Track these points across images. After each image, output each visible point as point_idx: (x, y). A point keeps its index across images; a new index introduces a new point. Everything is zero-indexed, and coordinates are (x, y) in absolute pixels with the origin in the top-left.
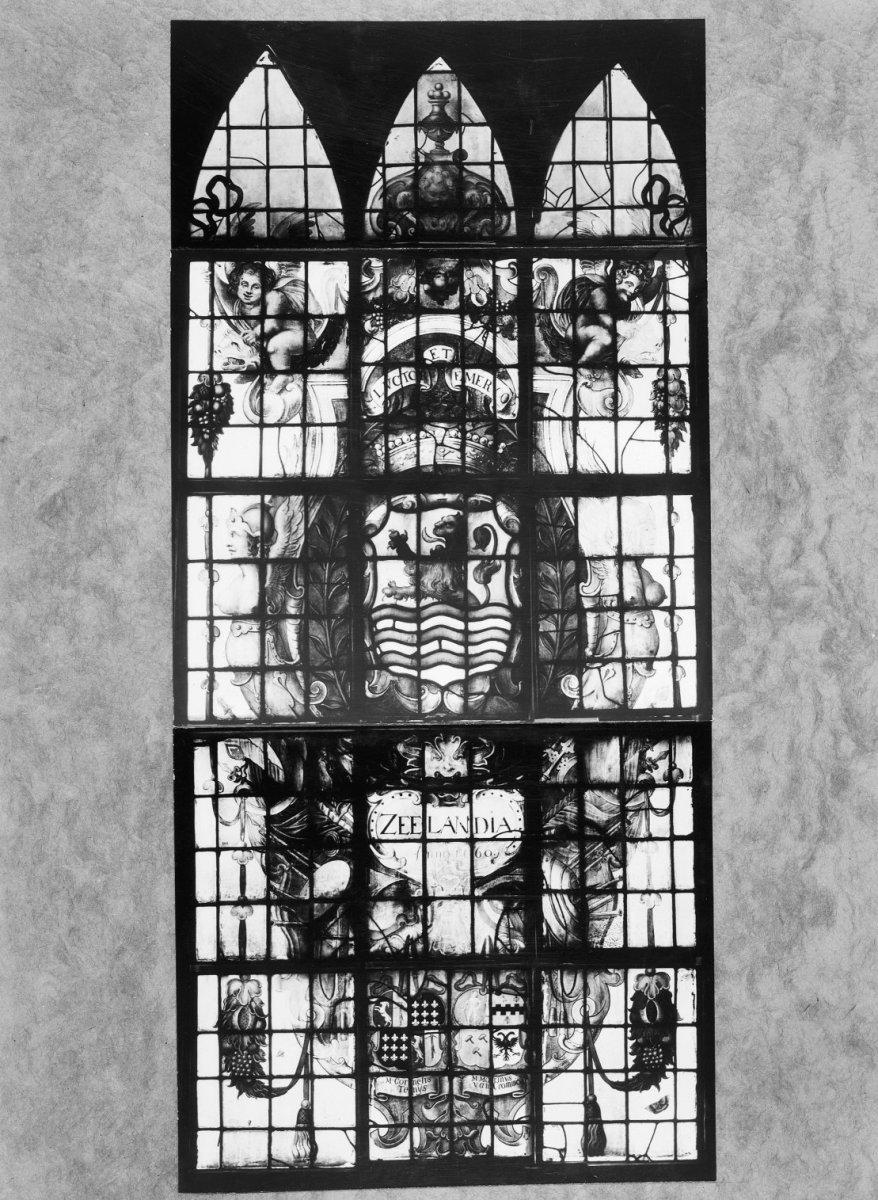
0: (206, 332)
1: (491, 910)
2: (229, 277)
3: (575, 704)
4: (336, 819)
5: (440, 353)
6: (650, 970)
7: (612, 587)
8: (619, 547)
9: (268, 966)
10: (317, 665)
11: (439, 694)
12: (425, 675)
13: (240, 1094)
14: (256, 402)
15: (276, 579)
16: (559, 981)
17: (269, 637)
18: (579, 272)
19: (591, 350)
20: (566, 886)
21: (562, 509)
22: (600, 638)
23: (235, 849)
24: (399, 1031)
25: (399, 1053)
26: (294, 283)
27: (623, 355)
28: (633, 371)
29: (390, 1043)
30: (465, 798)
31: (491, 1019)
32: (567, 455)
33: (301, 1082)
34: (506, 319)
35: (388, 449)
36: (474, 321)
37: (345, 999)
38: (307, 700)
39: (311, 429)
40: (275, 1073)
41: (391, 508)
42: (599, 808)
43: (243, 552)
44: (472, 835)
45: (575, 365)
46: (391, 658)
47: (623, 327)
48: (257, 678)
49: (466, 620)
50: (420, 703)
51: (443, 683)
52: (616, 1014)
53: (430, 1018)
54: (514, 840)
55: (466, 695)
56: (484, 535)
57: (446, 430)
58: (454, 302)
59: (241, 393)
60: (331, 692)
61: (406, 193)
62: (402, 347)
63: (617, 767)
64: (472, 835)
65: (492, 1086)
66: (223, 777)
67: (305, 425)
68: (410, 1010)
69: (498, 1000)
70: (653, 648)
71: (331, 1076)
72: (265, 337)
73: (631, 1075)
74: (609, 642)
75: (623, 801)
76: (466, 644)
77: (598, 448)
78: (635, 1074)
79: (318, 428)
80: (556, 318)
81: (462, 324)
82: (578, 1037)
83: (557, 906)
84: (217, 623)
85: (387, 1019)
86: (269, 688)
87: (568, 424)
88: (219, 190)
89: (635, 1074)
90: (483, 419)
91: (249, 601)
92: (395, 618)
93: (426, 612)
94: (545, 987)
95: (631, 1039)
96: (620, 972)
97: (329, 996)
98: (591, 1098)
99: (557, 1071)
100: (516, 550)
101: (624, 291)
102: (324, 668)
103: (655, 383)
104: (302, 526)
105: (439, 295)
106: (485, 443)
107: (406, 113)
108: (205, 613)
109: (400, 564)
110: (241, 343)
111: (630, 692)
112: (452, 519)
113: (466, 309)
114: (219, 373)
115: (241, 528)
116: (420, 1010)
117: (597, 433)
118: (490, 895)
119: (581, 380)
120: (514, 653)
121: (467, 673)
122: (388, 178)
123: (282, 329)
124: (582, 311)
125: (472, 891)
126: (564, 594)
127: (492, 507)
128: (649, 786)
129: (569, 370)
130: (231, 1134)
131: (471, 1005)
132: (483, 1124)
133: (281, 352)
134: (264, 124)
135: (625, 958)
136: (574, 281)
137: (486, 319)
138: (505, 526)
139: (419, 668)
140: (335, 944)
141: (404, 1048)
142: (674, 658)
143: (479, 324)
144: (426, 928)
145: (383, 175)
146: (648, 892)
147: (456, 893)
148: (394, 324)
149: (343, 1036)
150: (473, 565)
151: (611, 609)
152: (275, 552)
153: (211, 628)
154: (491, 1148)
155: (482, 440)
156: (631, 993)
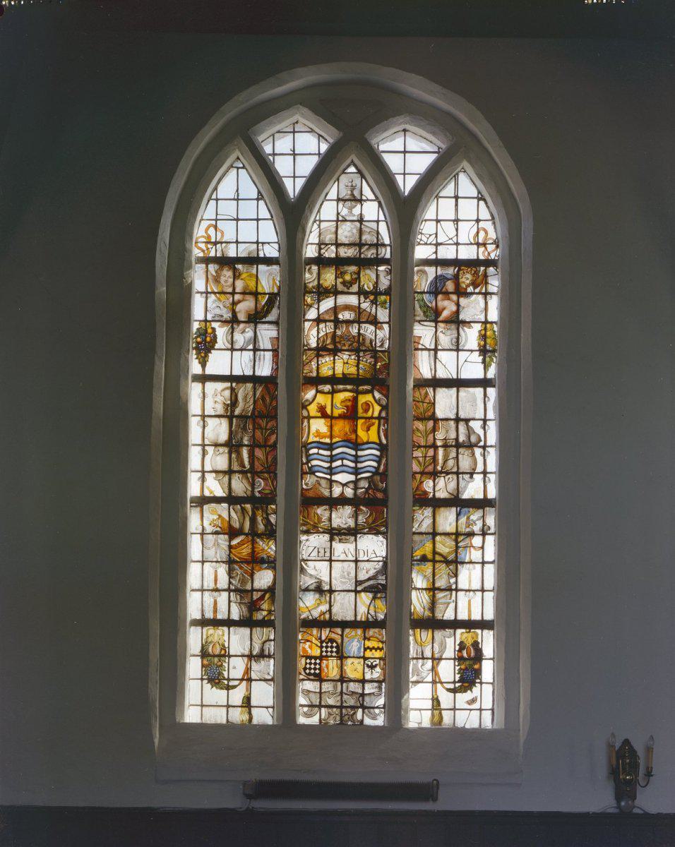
0: (204, 300)
1: (366, 598)
2: (216, 272)
3: (431, 495)
4: (266, 548)
5: (345, 315)
6: (468, 630)
7: (453, 435)
8: (457, 414)
9: (229, 623)
10: (259, 470)
11: (341, 488)
12: (335, 478)
13: (212, 687)
14: (229, 338)
15: (238, 426)
16: (419, 635)
17: (233, 456)
18: (439, 273)
19: (445, 314)
20: (424, 586)
21: (427, 394)
22: (445, 461)
23: (212, 562)
24: (316, 658)
25: (315, 669)
26: (251, 276)
27: (462, 317)
28: (467, 325)
29: (310, 664)
30: (353, 538)
31: (364, 653)
32: (431, 369)
33: (244, 683)
34: (383, 298)
35: (318, 365)
36: (366, 299)
37: (269, 640)
38: (253, 488)
39: (258, 353)
40: (231, 677)
41: (318, 391)
42: (445, 546)
43: (220, 411)
44: (356, 558)
45: (436, 322)
46: (316, 468)
47: (463, 301)
48: (227, 477)
49: (356, 450)
50: (331, 492)
51: (344, 482)
52: (450, 652)
53: (332, 652)
54: (379, 561)
55: (356, 489)
56: (367, 406)
57: (350, 356)
58: (355, 288)
59: (221, 332)
60: (266, 485)
61: (331, 236)
62: (326, 312)
63: (454, 524)
64: (356, 558)
65: (364, 688)
66: (206, 523)
67: (255, 350)
68: (321, 647)
69: (368, 644)
70: (473, 467)
71: (260, 680)
72: (234, 303)
73: (457, 685)
74: (451, 463)
75: (457, 542)
76: (356, 462)
77: (447, 366)
78: (459, 684)
79: (262, 353)
80: (426, 297)
81: (359, 300)
82: (429, 664)
83: (419, 597)
84: (207, 448)
85: (309, 651)
86: (233, 482)
87: (432, 352)
88: (212, 231)
89: (459, 684)
90: (369, 351)
91: (224, 437)
92: (319, 448)
93: (335, 446)
94: (411, 638)
95: (458, 666)
96: (452, 631)
97: (260, 638)
98: (435, 696)
99: (417, 682)
100: (383, 414)
101: (464, 282)
102: (262, 472)
103: (480, 331)
104: (252, 399)
105: (347, 284)
106: (370, 363)
107: (333, 194)
108: (200, 442)
109: (322, 421)
110: (222, 307)
111: (460, 490)
112: (350, 398)
113: (361, 293)
114: (210, 321)
115: (219, 399)
116: (327, 647)
117: (446, 358)
118: (365, 590)
119: (440, 330)
120: (382, 467)
121: (356, 477)
122: (321, 228)
123: (243, 300)
124: (441, 293)
125: (356, 587)
126: (427, 437)
127: (371, 392)
128: (472, 534)
129: (433, 324)
130: (207, 708)
131: (354, 643)
132: (358, 708)
133: (243, 312)
134: (236, 198)
135: (455, 624)
136: (436, 277)
137: (372, 297)
138: (378, 402)
139: (331, 474)
140: (265, 613)
141: (318, 666)
142: (485, 473)
143: (368, 300)
144: (330, 606)
145: (319, 226)
146: (469, 591)
147: (347, 589)
148: (323, 299)
149: (267, 659)
150: (360, 422)
151: (451, 446)
152: (237, 412)
153: (204, 450)
154: (362, 721)
155: (368, 361)
156: (458, 642)
